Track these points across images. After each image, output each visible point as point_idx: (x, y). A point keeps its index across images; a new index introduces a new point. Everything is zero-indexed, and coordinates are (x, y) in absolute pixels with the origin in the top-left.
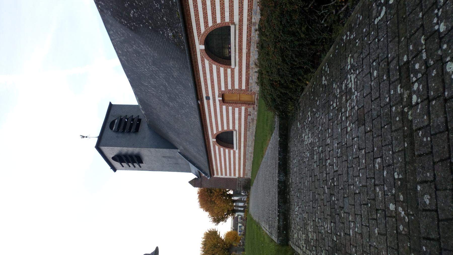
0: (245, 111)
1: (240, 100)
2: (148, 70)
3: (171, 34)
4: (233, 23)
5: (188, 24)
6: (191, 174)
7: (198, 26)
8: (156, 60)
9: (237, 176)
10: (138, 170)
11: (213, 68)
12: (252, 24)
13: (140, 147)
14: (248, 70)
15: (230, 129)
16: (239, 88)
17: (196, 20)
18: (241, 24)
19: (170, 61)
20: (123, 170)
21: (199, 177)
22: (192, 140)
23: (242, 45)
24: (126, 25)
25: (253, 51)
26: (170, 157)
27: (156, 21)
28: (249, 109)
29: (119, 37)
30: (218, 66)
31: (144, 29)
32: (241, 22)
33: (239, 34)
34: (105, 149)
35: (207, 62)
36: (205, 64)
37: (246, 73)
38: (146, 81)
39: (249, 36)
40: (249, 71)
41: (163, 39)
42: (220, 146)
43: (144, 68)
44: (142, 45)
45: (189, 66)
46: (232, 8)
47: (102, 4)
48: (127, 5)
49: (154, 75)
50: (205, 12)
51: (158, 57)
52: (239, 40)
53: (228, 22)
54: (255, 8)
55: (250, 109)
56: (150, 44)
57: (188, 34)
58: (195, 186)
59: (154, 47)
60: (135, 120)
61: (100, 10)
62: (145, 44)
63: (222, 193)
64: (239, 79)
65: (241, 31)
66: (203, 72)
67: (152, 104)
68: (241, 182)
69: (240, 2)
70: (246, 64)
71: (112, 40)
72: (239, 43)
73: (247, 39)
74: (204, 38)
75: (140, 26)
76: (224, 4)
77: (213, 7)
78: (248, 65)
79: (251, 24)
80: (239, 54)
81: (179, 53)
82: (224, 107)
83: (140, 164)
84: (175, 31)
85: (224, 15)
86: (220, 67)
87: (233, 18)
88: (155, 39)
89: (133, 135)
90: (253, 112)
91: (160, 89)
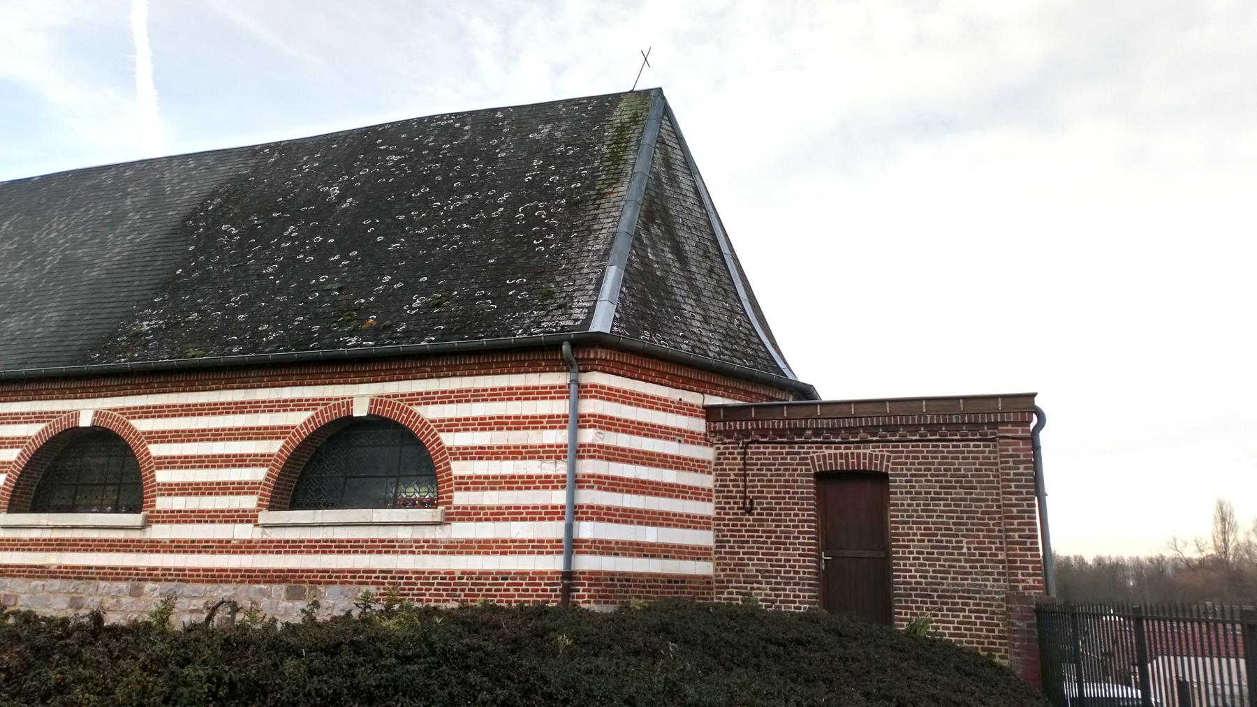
2: (52, 242)
3: (145, 326)
4: (149, 522)
5: (162, 380)
8: (76, 272)
12: (136, 583)
17: (174, 406)
18: (143, 547)
19: (60, 314)
23: (73, 551)
24: (203, 207)
25: (46, 588)
27: (194, 290)
29: (176, 181)
30: (14, 467)
33: (113, 541)
35: (31, 430)
36: (26, 422)
41: (138, 301)
42: (297, 440)
43: (59, 231)
47: (270, 158)
48: (253, 221)
51: (86, 278)
52: (94, 540)
53: (154, 506)
54: (185, 589)
57: (131, 377)
59: (120, 270)
61: (257, 148)
62: (136, 248)
72: (81, 540)
73: (90, 568)
74: (114, 426)
75: (191, 245)
76: (210, 494)
77: (204, 462)
80: (44, 540)
84: (149, 341)
85: (176, 495)
87: (164, 522)
88: (142, 278)
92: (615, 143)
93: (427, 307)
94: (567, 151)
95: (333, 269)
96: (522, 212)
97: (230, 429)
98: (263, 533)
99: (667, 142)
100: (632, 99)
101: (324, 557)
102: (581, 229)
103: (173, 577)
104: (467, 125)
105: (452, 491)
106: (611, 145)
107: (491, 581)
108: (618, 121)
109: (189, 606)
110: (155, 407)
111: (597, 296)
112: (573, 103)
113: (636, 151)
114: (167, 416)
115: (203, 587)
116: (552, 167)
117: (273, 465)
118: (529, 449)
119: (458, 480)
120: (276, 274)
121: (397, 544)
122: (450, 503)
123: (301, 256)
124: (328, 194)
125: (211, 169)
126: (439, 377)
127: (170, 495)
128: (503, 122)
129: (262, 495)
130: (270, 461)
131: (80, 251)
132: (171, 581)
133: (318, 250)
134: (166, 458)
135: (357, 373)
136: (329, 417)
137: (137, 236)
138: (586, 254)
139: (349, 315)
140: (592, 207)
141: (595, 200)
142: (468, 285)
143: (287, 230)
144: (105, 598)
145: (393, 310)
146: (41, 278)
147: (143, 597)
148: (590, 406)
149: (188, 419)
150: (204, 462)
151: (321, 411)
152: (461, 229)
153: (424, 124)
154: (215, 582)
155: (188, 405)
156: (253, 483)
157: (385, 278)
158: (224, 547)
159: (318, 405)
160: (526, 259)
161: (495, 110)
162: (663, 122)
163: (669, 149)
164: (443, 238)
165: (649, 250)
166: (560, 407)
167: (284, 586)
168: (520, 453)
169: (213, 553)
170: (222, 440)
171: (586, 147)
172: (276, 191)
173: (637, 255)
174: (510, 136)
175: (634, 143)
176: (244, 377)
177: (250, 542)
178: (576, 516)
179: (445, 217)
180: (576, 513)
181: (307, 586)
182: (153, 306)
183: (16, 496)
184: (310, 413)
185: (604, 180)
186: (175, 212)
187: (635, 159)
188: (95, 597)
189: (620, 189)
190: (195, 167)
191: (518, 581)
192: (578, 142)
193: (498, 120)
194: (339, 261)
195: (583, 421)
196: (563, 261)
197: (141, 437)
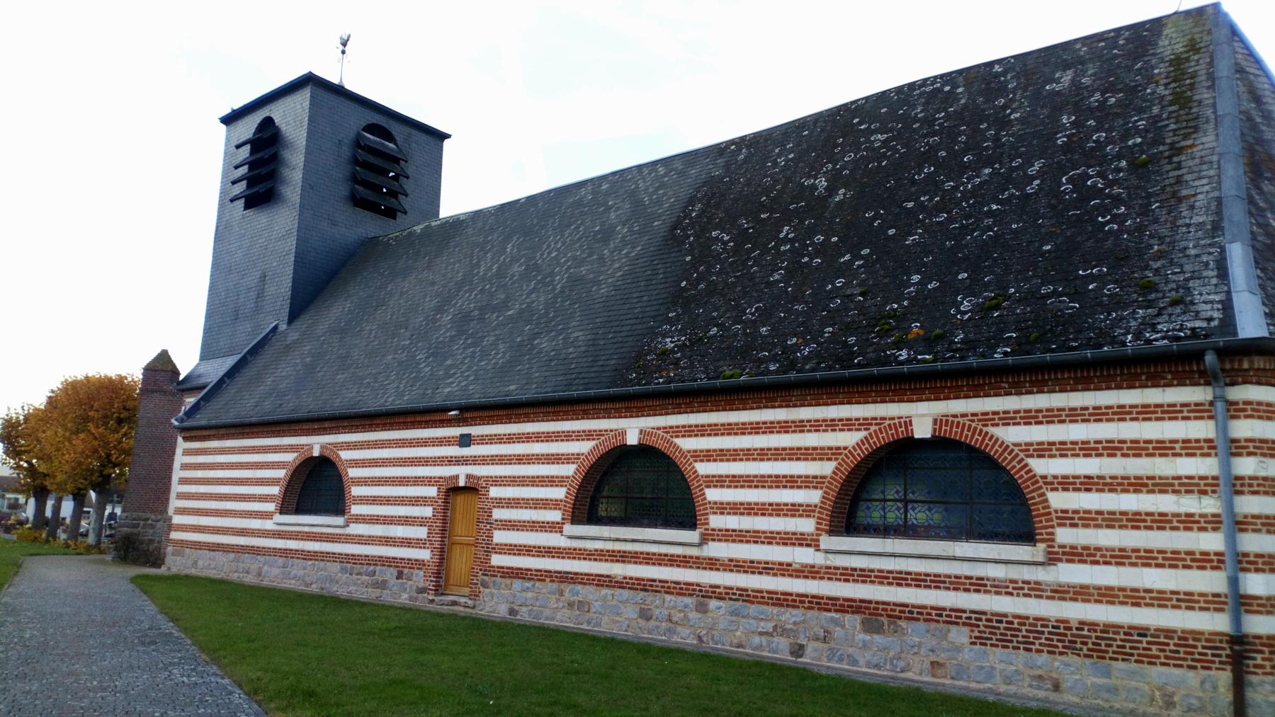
0: (416, 560)
1: (454, 547)
2: (555, 262)
4: (705, 539)
6: (196, 360)
7: (698, 431)
9: (177, 520)
10: (223, 192)
11: (566, 466)
13: (302, 206)
14: (556, 577)
15: (353, 507)
16: (497, 545)
17: (716, 425)
18: (703, 563)
20: (226, 145)
21: (181, 387)
22: (320, 375)
23: (636, 563)
25: (615, 597)
26: (260, 295)
27: (705, 303)
28: (421, 573)
29: (651, 190)
31: (677, 264)
32: (707, 564)
33: (672, 556)
34: (302, 99)
35: (584, 447)
37: (546, 571)
38: (519, 251)
39: (663, 587)
40: (553, 581)
42: (292, 469)
43: (558, 250)
44: (631, 253)
45: (574, 393)
46: (752, 539)
47: (739, 155)
49: (539, 278)
50: (739, 455)
51: (597, 296)
52: (654, 554)
53: (708, 524)
54: (751, 610)
55: (420, 578)
56: (632, 276)
58: (150, 370)
60: (394, 200)
62: (634, 262)
63: (113, 460)
64: (525, 546)
65: (680, 561)
66: (553, 433)
67: (444, 258)
68: (152, 527)
69: (770, 566)
70: (576, 574)
71: (640, 167)
72: (642, 553)
74: (660, 445)
75: (686, 255)
76: (763, 515)
78: (572, 578)
79: (703, 596)
80: (608, 551)
81: (613, 362)
82: (432, 491)
83: (243, 201)
85: (729, 514)
86: (569, 489)
87: (720, 540)
88: (650, 293)
89: (344, 190)
90: (411, 586)
91: (496, 291)
92: (1174, 81)
93: (983, 310)
94: (1106, 100)
95: (846, 270)
96: (1068, 183)
97: (776, 449)
98: (826, 559)
99: (1248, 69)
100: (1181, 22)
101: (900, 589)
102: (1163, 197)
103: (737, 597)
104: (959, 87)
105: (1053, 527)
106: (1169, 83)
107: (1122, 637)
108: (1169, 52)
109: (758, 628)
110: (697, 426)
111: (1228, 285)
112: (1095, 39)
113: (1211, 88)
114: (709, 435)
115: (770, 609)
116: (1092, 122)
117: (827, 487)
118: (1158, 481)
119: (1060, 514)
120: (786, 279)
121: (988, 583)
122: (1053, 540)
123: (806, 259)
124: (814, 187)
125: (681, 173)
126: (1019, 394)
127: (722, 513)
128: (1005, 77)
129: (819, 518)
130: (823, 483)
131: (582, 269)
132: (735, 600)
133: (820, 251)
134: (714, 476)
135: (914, 391)
136: (886, 437)
137: (631, 250)
138: (1184, 229)
139: (887, 324)
140: (1169, 167)
141: (1170, 157)
142: (1026, 280)
143: (782, 232)
144: (672, 611)
145: (938, 315)
146: (555, 297)
147: (709, 614)
148: (1244, 429)
149: (731, 438)
150: (753, 481)
151: (875, 431)
152: (990, 210)
153: (905, 94)
154: (782, 605)
155: (730, 424)
156: (807, 506)
157: (914, 277)
158: (784, 569)
159: (871, 424)
160: (1097, 242)
161: (990, 64)
162: (1235, 44)
163: (1252, 77)
164: (971, 224)
165: (1269, 215)
166: (1201, 429)
167: (858, 618)
168: (1146, 485)
169: (775, 575)
170: (769, 459)
171: (1132, 91)
172: (756, 190)
173: (1259, 225)
174: (1020, 92)
175: (1203, 78)
176: (786, 396)
177: (813, 566)
178: (1240, 566)
179: (965, 198)
180: (1240, 562)
181: (884, 620)
182: (670, 322)
183: (577, 508)
184: (862, 434)
185: (1174, 130)
186: (660, 222)
187: (1215, 97)
188: (663, 610)
189: (1204, 140)
190: (665, 173)
191: (1162, 640)
192: (1119, 87)
193: (997, 75)
194: (851, 262)
195: (1236, 448)
196: (1152, 241)
197: (686, 456)
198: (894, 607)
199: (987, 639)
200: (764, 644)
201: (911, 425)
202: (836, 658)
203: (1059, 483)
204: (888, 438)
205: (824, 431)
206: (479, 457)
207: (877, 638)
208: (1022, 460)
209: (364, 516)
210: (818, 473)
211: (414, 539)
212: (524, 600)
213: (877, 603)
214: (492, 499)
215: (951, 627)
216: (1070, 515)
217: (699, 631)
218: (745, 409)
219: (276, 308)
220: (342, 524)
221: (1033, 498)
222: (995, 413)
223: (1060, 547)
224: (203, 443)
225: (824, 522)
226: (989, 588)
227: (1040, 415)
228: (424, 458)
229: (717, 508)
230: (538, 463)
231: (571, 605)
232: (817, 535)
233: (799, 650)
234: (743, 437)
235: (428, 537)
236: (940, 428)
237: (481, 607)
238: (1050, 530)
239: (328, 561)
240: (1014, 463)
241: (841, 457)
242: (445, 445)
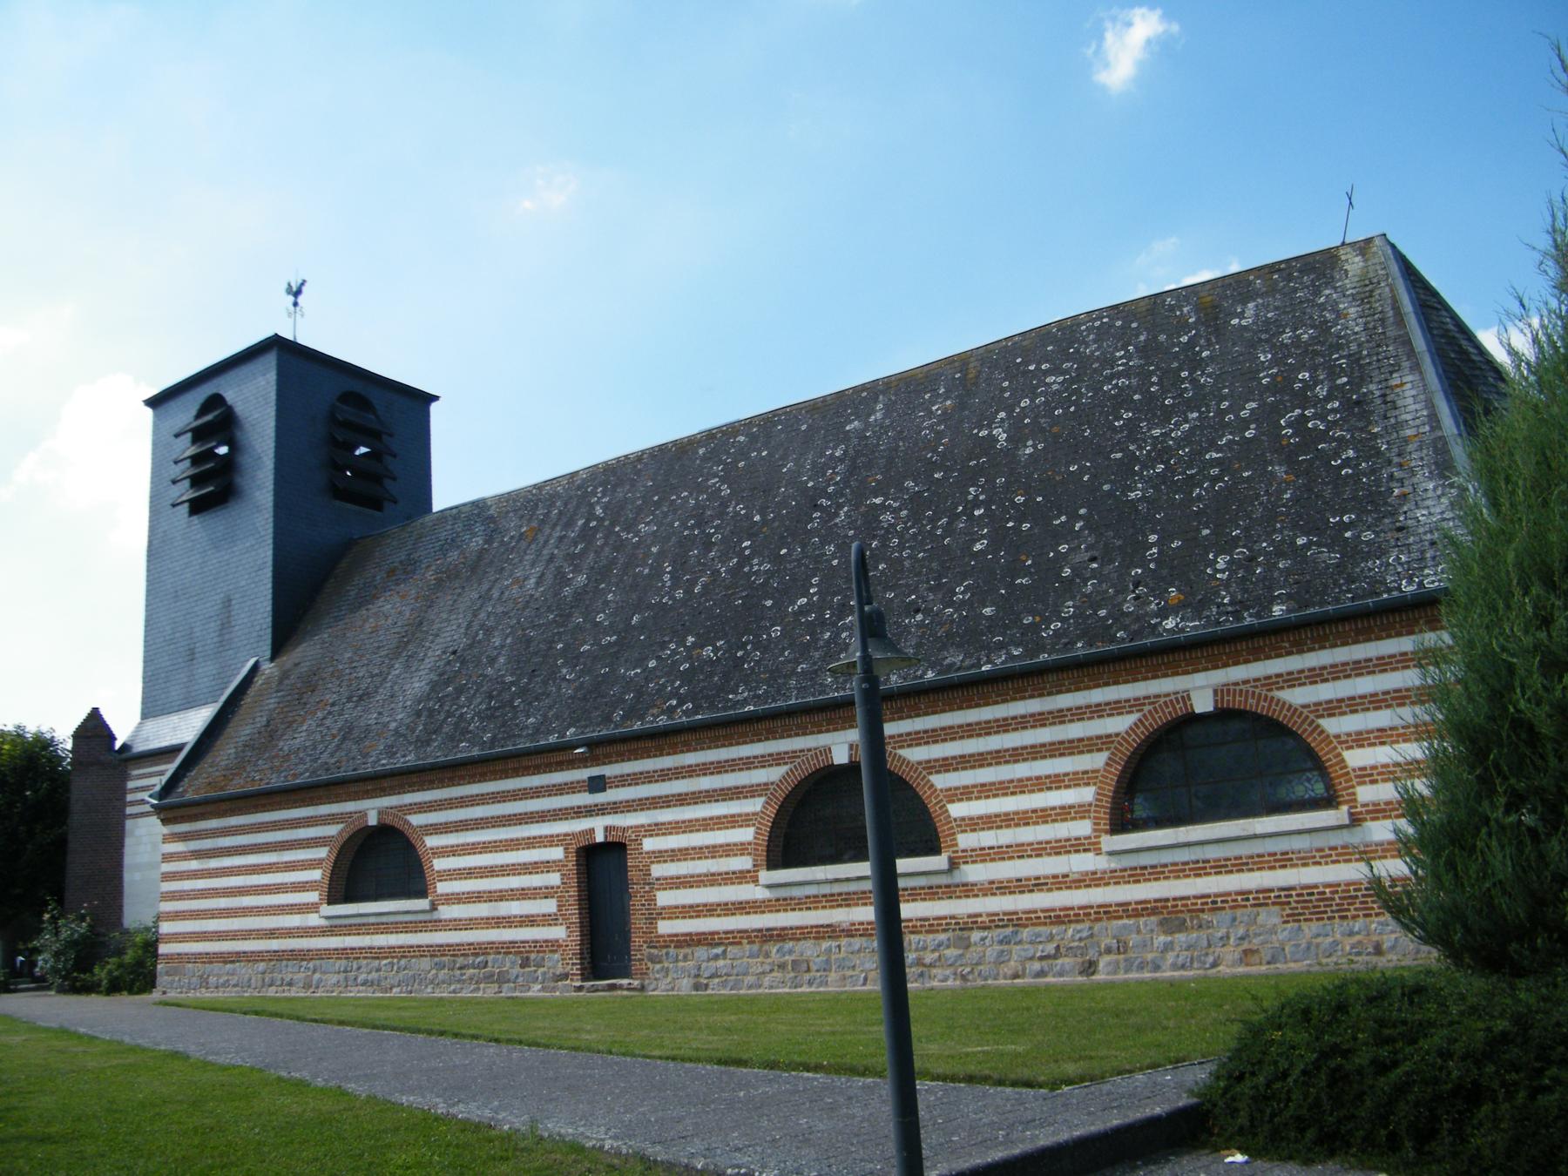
0: (546, 941)
15: (439, 885)
16: (664, 908)
25: (843, 949)
34: (270, 360)
42: (338, 846)
53: (956, 845)
58: (81, 734)
69: (1042, 881)
70: (784, 929)
82: (557, 853)
95: (1066, 533)
98: (1109, 861)
103: (1005, 923)
105: (1353, 787)
110: (926, 732)
121: (1294, 856)
122: (1355, 800)
126: (1301, 652)
127: (974, 830)
129: (1095, 818)
132: (1003, 926)
136: (1161, 718)
151: (1150, 712)
156: (1080, 806)
159: (1144, 704)
169: (1050, 890)
177: (1094, 873)
181: (1187, 916)
197: (917, 769)
198: (1194, 901)
199: (1300, 914)
200: (1046, 969)
201: (1190, 699)
202: (1134, 968)
203: (1353, 741)
204: (1166, 717)
205: (1089, 719)
206: (621, 802)
207: (1181, 937)
208: (1313, 721)
209: (458, 894)
210: (1088, 767)
211: (538, 916)
212: (714, 971)
213: (1175, 899)
214: (647, 853)
215: (1260, 909)
216: (1369, 772)
217: (960, 970)
218: (987, 704)
219: (252, 641)
220: (428, 908)
221: (1330, 760)
222: (1278, 676)
223: (1364, 805)
224: (193, 824)
225: (1102, 822)
226: (1295, 862)
227: (1325, 672)
228: (537, 813)
229: (966, 825)
230: (710, 801)
231: (782, 966)
232: (1095, 837)
233: (1090, 967)
234: (988, 738)
235: (559, 911)
236: (1222, 699)
237: (652, 987)
238: (1351, 791)
239: (413, 957)
240: (1305, 726)
241: (1113, 746)
242: (568, 793)
